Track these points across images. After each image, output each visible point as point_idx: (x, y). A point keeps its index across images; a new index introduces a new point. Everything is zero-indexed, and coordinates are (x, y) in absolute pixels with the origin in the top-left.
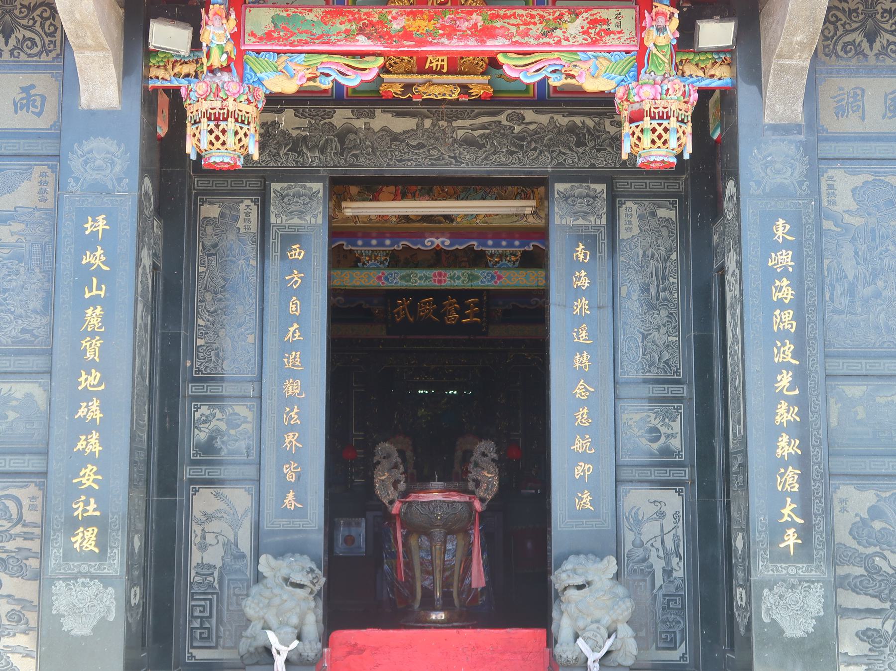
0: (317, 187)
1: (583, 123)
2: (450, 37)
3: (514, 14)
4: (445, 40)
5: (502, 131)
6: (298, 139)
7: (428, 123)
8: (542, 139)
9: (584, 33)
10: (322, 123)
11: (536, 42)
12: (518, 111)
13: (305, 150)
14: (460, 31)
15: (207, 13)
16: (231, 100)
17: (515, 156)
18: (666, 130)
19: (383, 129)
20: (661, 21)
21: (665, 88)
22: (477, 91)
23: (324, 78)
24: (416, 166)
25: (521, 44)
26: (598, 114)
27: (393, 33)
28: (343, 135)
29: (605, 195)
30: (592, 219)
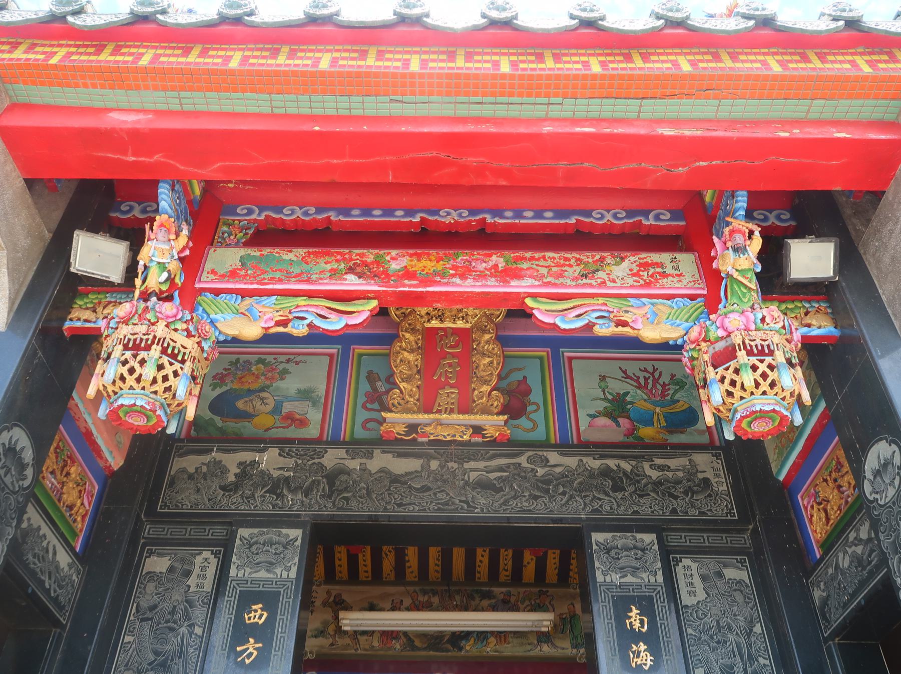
0: (296, 534)
1: (618, 466)
2: (463, 277)
3: (544, 257)
4: (457, 280)
5: (523, 474)
6: (279, 479)
7: (434, 465)
8: (571, 482)
9: (633, 275)
10: (310, 463)
11: (574, 283)
12: (540, 453)
13: (285, 492)
14: (476, 271)
15: (151, 229)
16: (161, 325)
17: (540, 501)
18: (771, 367)
19: (382, 470)
20: (739, 239)
21: (760, 316)
22: (492, 432)
23: (297, 322)
24: (419, 511)
25: (555, 285)
26: (635, 458)
27: (390, 272)
28: (333, 476)
29: (656, 547)
30: (644, 575)
